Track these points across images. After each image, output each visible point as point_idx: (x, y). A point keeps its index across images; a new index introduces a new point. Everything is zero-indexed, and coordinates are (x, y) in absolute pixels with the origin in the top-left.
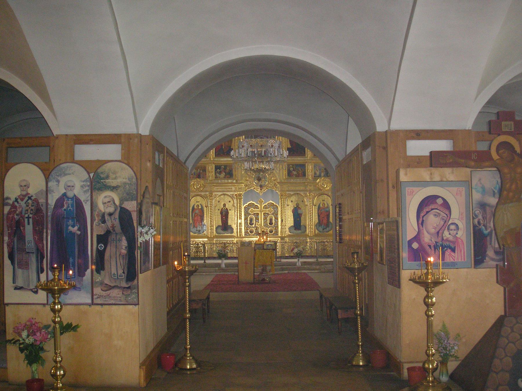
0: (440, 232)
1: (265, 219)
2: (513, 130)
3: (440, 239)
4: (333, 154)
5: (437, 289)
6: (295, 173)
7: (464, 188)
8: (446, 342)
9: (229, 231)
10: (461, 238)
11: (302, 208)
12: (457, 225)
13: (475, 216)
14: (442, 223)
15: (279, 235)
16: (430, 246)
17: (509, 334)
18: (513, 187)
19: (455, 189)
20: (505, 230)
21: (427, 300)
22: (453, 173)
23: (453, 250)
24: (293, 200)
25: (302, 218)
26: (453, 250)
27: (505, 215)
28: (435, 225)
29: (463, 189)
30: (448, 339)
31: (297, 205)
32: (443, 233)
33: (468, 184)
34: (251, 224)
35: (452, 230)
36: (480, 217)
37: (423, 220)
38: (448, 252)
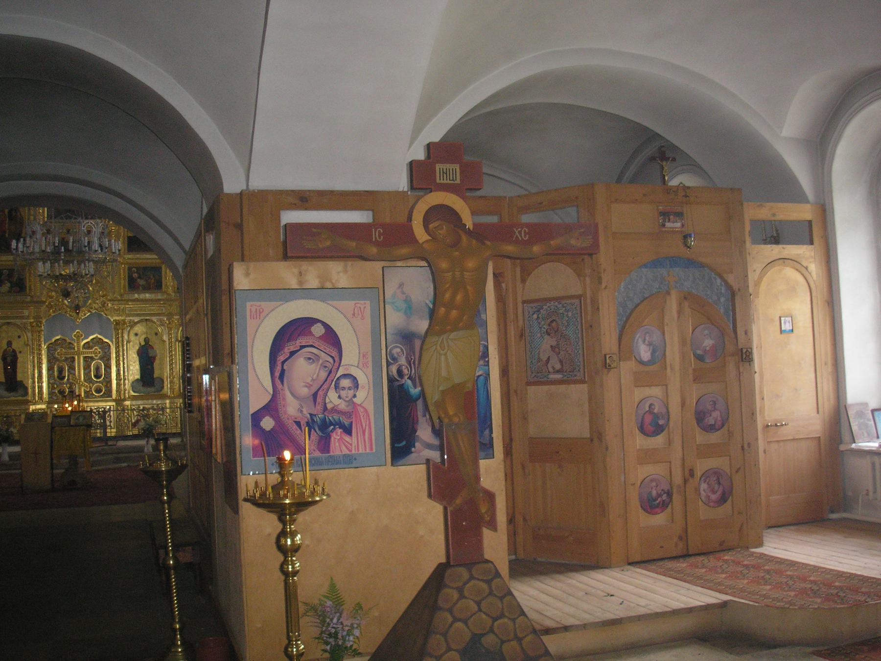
0: (320, 393)
1: (87, 367)
2: (458, 181)
3: (319, 407)
4: (176, 239)
5: (303, 517)
6: (142, 282)
7: (368, 302)
8: (335, 620)
9: (20, 392)
10: (363, 405)
11: (156, 347)
12: (355, 378)
13: (392, 359)
14: (323, 374)
15: (114, 396)
16: (298, 424)
17: (455, 604)
18: (459, 297)
19: (348, 305)
20: (441, 388)
21: (283, 541)
22: (345, 271)
23: (348, 431)
24: (139, 332)
25: (156, 364)
26: (348, 431)
27: (443, 358)
28: (309, 380)
29: (367, 306)
30: (340, 617)
31: (146, 340)
32: (326, 395)
33: (376, 294)
34: (61, 377)
35: (344, 389)
36: (403, 361)
37: (283, 371)
38: (337, 435)
